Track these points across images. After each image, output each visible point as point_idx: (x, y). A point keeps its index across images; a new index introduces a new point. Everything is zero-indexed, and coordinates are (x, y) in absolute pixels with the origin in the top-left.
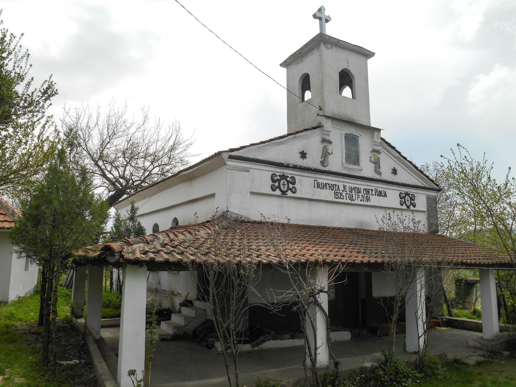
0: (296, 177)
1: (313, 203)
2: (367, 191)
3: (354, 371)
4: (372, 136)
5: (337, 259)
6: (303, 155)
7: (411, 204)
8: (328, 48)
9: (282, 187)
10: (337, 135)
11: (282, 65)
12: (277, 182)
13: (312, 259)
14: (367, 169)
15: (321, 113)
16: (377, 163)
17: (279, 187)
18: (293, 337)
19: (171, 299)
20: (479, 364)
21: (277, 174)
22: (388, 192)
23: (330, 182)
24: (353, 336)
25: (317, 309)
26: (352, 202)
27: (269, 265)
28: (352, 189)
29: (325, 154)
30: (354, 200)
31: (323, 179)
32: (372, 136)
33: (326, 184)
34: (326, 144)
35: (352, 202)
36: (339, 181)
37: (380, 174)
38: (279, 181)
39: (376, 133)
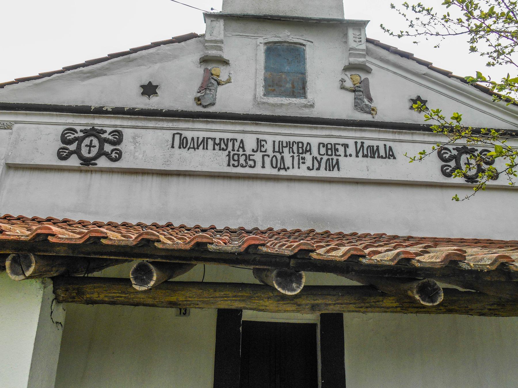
2: (332, 149)
12: (76, 144)
17: (78, 152)
21: (78, 128)
22: (398, 149)
23: (218, 136)
26: (282, 173)
28: (279, 148)
30: (286, 169)
31: (196, 130)
33: (205, 141)
35: (282, 173)
36: (244, 132)
37: (372, 111)
38: (80, 140)
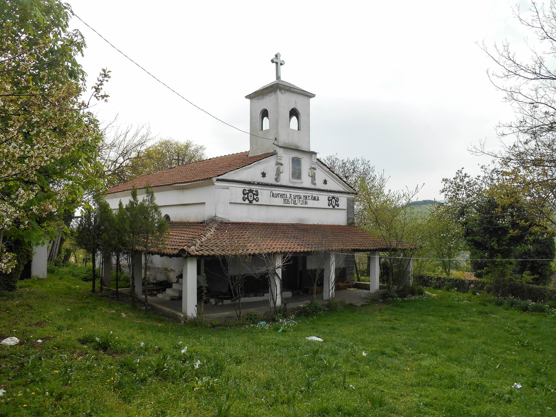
0: (259, 191)
1: (269, 207)
2: (306, 197)
3: (294, 309)
4: (311, 158)
5: (287, 250)
6: (264, 175)
7: (336, 204)
8: (282, 93)
9: (250, 198)
10: (286, 158)
11: (247, 97)
13: (275, 251)
14: (306, 182)
15: (276, 142)
16: (313, 177)
17: (248, 198)
18: (256, 296)
19: (166, 274)
20: (363, 305)
21: (247, 189)
23: (281, 193)
24: (293, 295)
25: (276, 278)
27: (254, 255)
29: (278, 173)
31: (277, 191)
32: (311, 158)
34: (279, 166)
37: (315, 184)
38: (248, 194)
39: (314, 155)
